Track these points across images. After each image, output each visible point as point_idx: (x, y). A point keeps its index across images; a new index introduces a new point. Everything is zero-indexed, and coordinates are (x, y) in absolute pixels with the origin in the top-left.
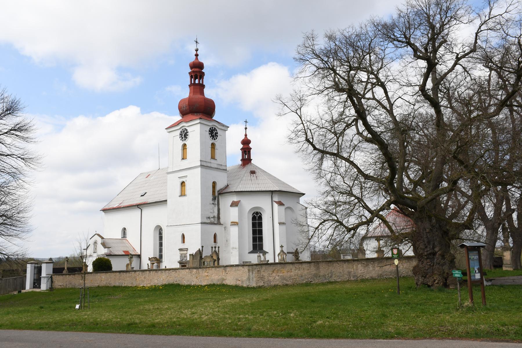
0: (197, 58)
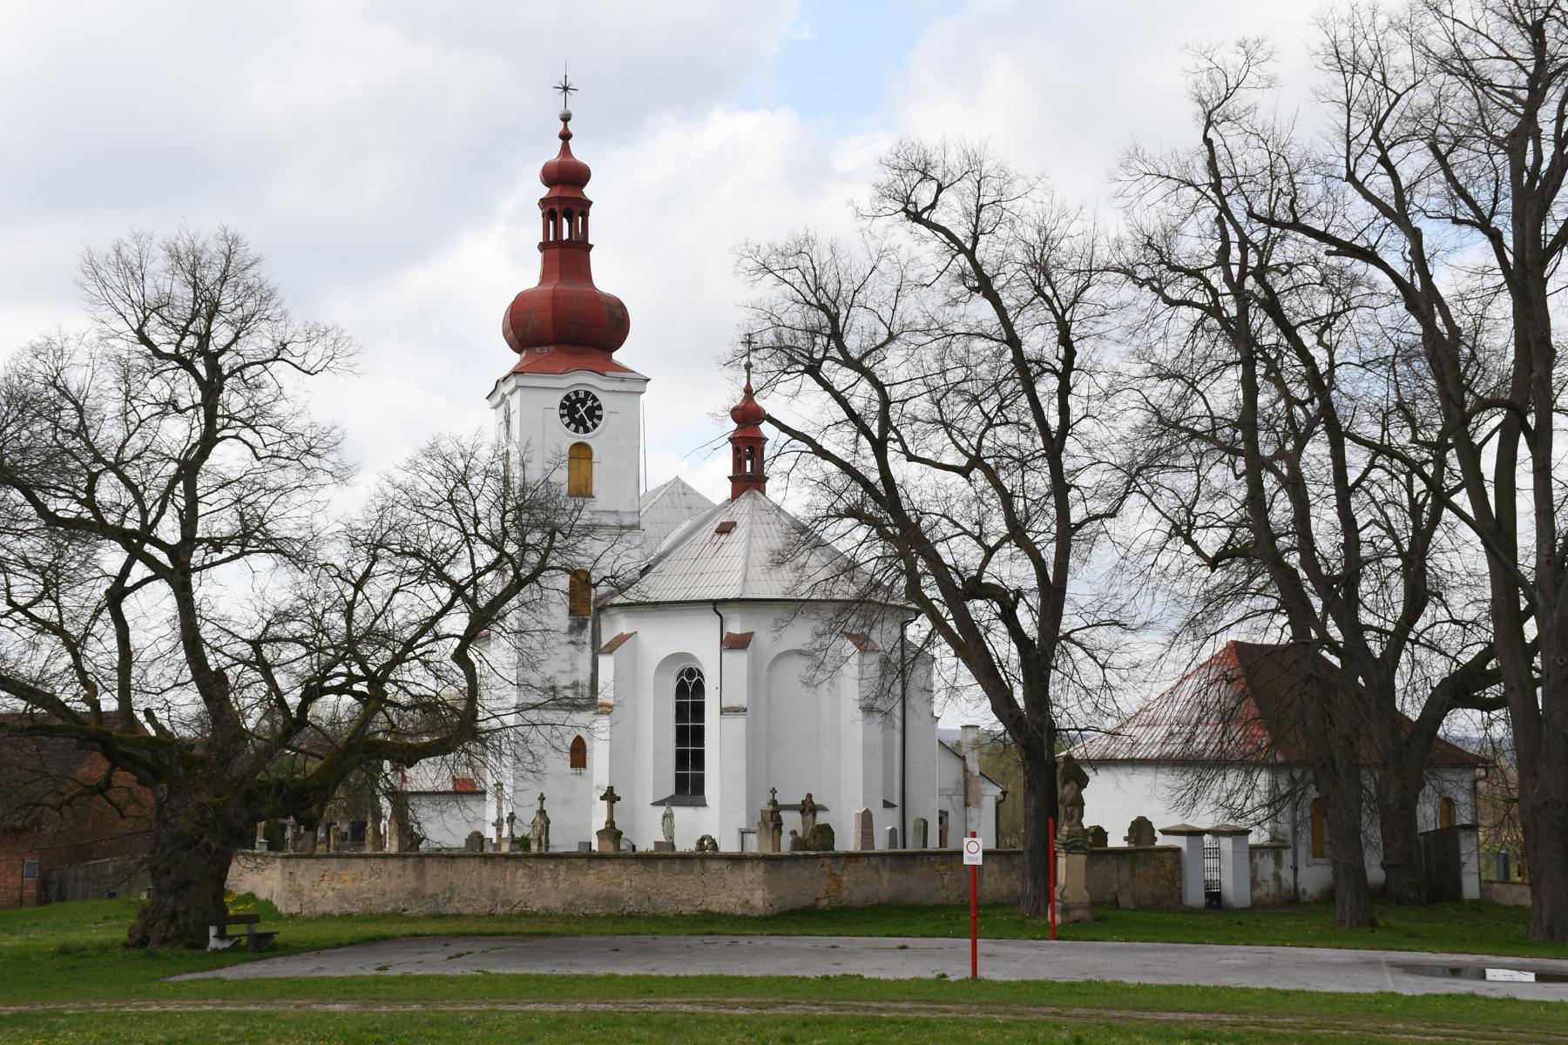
0: (566, 150)
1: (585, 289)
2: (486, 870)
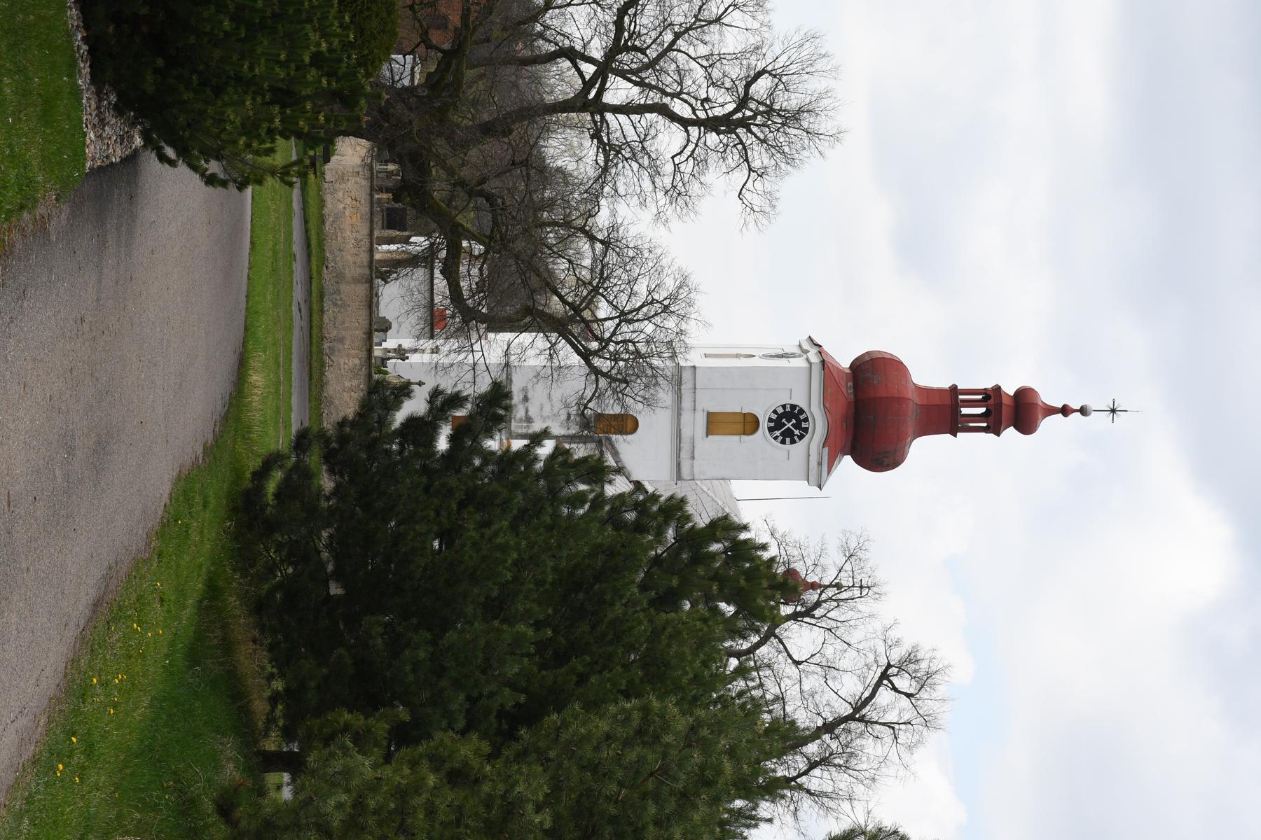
0: (1051, 411)
1: (911, 425)
2: (360, 334)
